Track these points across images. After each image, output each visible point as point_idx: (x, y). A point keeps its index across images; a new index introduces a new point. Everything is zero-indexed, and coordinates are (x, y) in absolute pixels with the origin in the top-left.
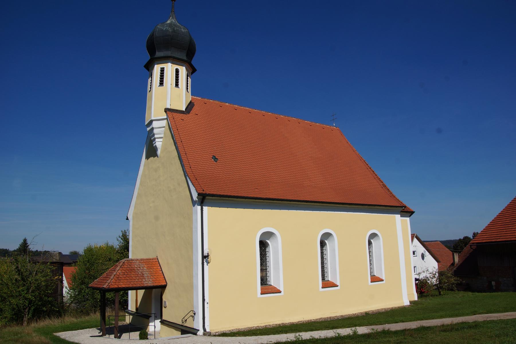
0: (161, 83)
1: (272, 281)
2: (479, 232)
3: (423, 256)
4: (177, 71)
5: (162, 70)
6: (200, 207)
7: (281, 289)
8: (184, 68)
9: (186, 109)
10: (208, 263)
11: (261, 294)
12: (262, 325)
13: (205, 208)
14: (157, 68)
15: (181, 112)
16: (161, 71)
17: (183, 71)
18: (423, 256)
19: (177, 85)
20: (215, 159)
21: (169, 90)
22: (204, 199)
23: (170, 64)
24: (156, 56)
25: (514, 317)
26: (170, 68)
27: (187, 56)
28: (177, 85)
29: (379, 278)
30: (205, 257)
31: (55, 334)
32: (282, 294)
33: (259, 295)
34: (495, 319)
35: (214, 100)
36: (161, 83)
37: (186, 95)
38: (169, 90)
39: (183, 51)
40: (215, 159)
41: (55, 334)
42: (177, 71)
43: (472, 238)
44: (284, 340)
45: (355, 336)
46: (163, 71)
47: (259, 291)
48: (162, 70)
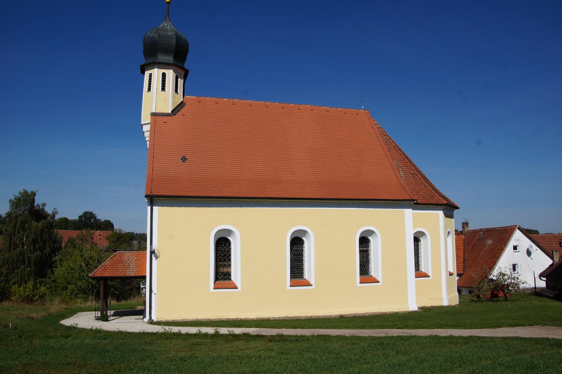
0: (149, 89)
1: (423, 269)
2: (541, 233)
3: (529, 253)
4: (164, 75)
5: (151, 75)
6: (149, 208)
8: (171, 71)
9: (172, 112)
10: (157, 257)
11: (214, 288)
12: (213, 318)
13: (155, 208)
14: (147, 73)
15: (167, 115)
17: (170, 74)
18: (529, 253)
19: (163, 89)
20: (184, 159)
21: (159, 93)
22: (153, 200)
23: (156, 70)
24: (158, 61)
25: (561, 338)
26: (156, 73)
27: (174, 58)
28: (163, 89)
29: (375, 278)
30: (152, 252)
34: (395, 335)
35: (210, 97)
36: (149, 89)
37: (173, 97)
38: (159, 93)
39: (175, 54)
40: (184, 159)
42: (164, 75)
44: (334, 334)
45: (217, 335)
47: (288, 283)
48: (151, 75)
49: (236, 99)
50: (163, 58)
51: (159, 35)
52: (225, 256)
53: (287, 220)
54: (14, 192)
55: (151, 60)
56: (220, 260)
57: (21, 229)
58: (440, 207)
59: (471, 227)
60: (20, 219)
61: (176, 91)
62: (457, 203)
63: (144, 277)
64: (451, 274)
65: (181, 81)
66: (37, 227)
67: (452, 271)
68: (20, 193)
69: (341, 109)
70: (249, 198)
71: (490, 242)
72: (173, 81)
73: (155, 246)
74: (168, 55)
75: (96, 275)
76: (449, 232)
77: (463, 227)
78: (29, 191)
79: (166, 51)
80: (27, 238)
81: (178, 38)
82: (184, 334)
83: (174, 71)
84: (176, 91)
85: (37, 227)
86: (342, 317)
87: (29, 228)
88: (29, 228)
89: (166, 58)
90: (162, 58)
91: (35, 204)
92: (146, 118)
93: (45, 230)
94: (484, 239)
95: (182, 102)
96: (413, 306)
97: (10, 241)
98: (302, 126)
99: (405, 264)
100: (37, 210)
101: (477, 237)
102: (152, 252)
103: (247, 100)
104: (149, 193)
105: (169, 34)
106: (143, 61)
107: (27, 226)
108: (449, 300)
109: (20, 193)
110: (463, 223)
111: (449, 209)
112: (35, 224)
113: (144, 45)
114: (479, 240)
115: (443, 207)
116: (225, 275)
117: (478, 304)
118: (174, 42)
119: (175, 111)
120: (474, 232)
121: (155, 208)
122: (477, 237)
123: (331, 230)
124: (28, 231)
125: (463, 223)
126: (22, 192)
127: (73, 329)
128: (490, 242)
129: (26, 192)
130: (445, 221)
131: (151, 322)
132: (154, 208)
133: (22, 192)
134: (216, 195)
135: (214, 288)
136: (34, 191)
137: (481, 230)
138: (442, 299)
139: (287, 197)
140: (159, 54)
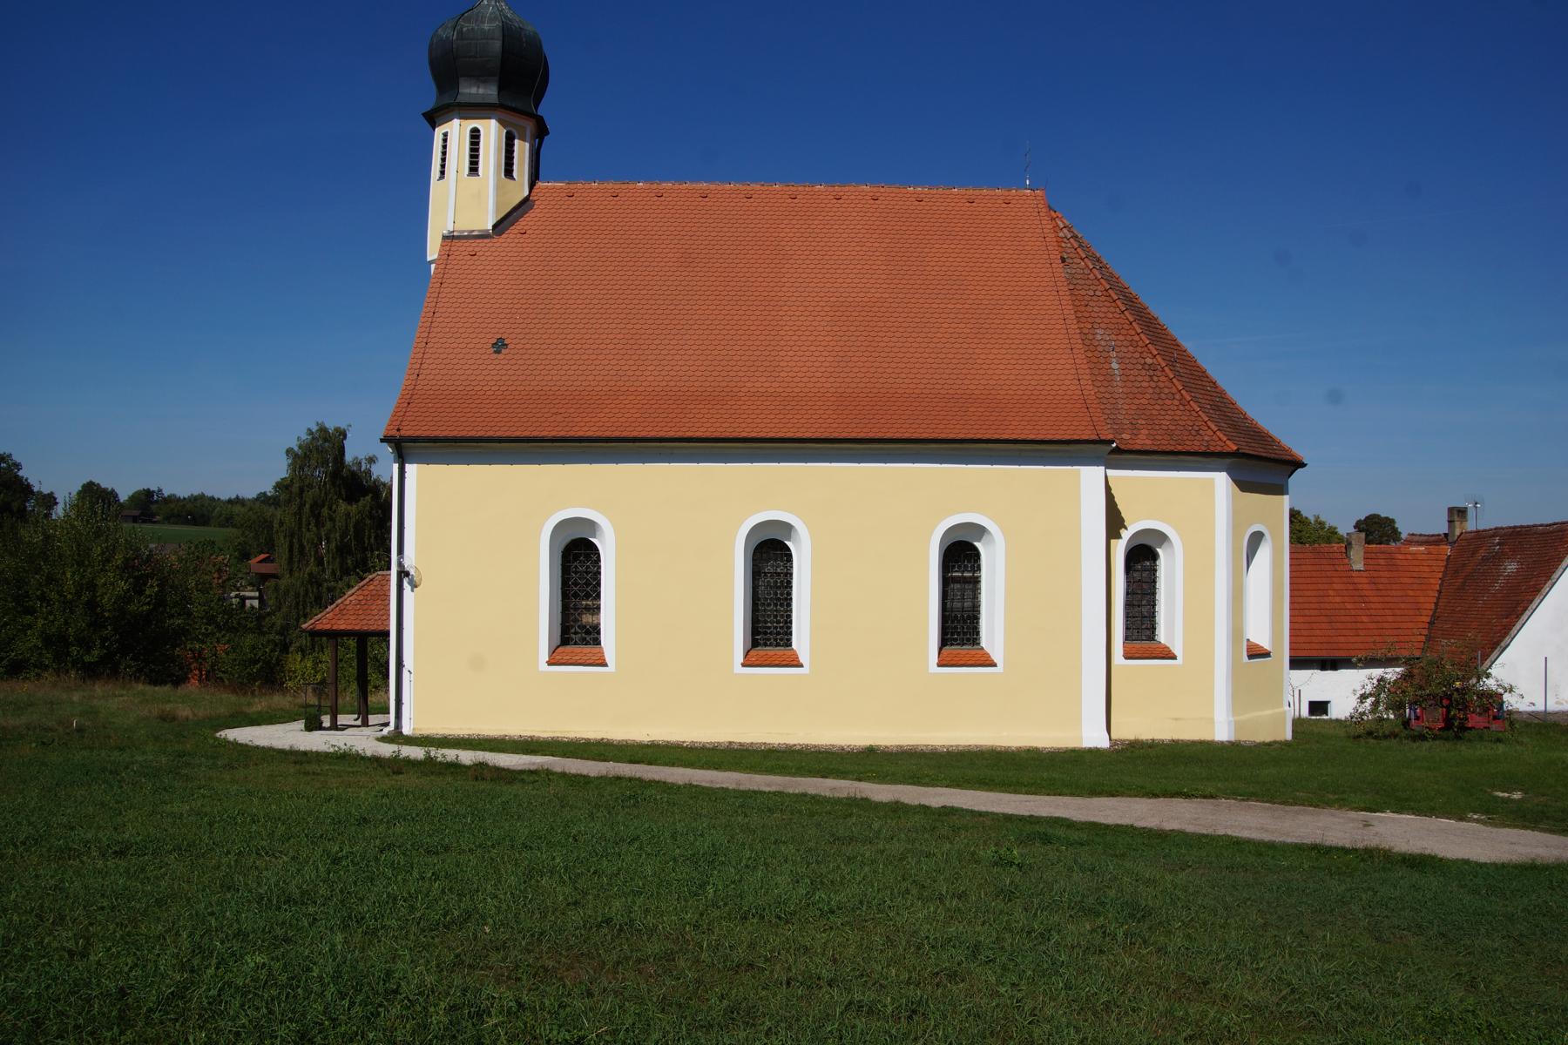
5: (445, 135)
6: (396, 467)
7: (1177, 651)
9: (495, 227)
10: (414, 586)
11: (550, 663)
12: (545, 735)
13: (411, 469)
15: (484, 236)
16: (472, 137)
17: (491, 131)
19: (474, 169)
21: (467, 181)
23: (456, 122)
24: (460, 99)
26: (456, 130)
28: (474, 169)
31: (233, 734)
32: (1179, 661)
33: (543, 667)
35: (602, 181)
37: (498, 187)
39: (514, 82)
41: (233, 734)
43: (1404, 536)
45: (429, 760)
46: (478, 137)
48: (445, 135)
49: (667, 180)
50: (474, 90)
51: (461, 32)
52: (588, 584)
53: (929, 497)
54: (294, 434)
55: (447, 100)
56: (576, 595)
57: (313, 522)
58: (1219, 460)
59: (1471, 525)
60: (309, 496)
61: (509, 172)
62: (1300, 451)
63: (387, 634)
64: (1256, 653)
65: (522, 149)
66: (348, 515)
67: (1265, 643)
68: (310, 432)
69: (963, 191)
70: (500, 440)
71: (1511, 567)
72: (499, 149)
73: (410, 561)
74: (484, 82)
75: (319, 627)
76: (1256, 539)
77: (1451, 522)
78: (331, 425)
79: (479, 74)
80: (328, 542)
81: (510, 34)
82: (468, 768)
83: (501, 122)
84: (509, 172)
85: (348, 515)
86: (871, 751)
87: (332, 519)
88: (332, 519)
89: (481, 91)
90: (471, 91)
91: (348, 458)
92: (433, 252)
93: (368, 522)
94: (1498, 558)
95: (526, 200)
96: (1094, 737)
97: (291, 550)
98: (830, 244)
99: (1091, 622)
100: (353, 474)
101: (1482, 553)
102: (403, 574)
103: (698, 181)
104: (394, 433)
105: (486, 26)
106: (430, 102)
107: (325, 511)
108: (1238, 726)
109: (310, 432)
110: (1451, 510)
111: (1261, 465)
112: (343, 507)
113: (431, 63)
114: (1485, 559)
115: (1228, 461)
116: (588, 632)
117: (1439, 750)
118: (497, 45)
119: (500, 226)
120: (1480, 536)
121: (411, 469)
122: (1482, 553)
123: (865, 527)
124: (329, 525)
125: (1451, 510)
126: (315, 429)
127: (226, 741)
128: (1511, 567)
129: (323, 430)
130: (1234, 503)
131: (397, 737)
132: (408, 467)
133: (315, 429)
134: (671, 434)
135: (550, 663)
136: (343, 426)
137: (1496, 532)
138: (1211, 721)
139: (844, 435)
140: (462, 80)
